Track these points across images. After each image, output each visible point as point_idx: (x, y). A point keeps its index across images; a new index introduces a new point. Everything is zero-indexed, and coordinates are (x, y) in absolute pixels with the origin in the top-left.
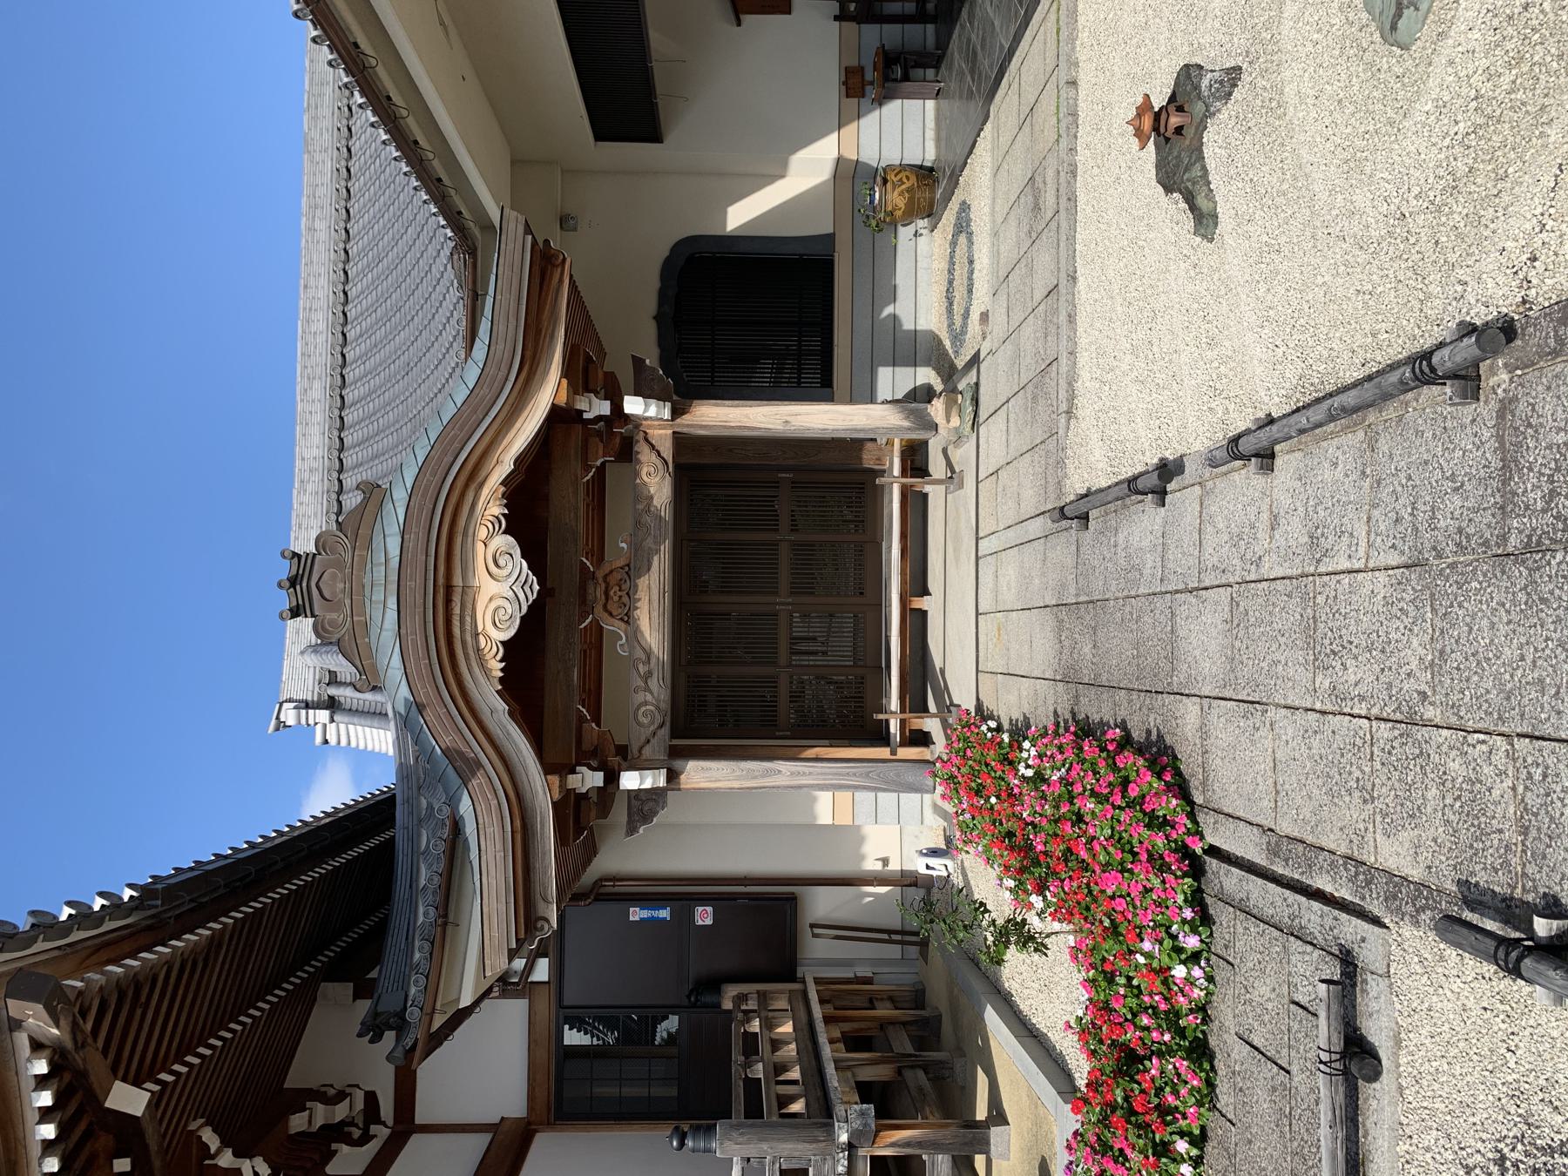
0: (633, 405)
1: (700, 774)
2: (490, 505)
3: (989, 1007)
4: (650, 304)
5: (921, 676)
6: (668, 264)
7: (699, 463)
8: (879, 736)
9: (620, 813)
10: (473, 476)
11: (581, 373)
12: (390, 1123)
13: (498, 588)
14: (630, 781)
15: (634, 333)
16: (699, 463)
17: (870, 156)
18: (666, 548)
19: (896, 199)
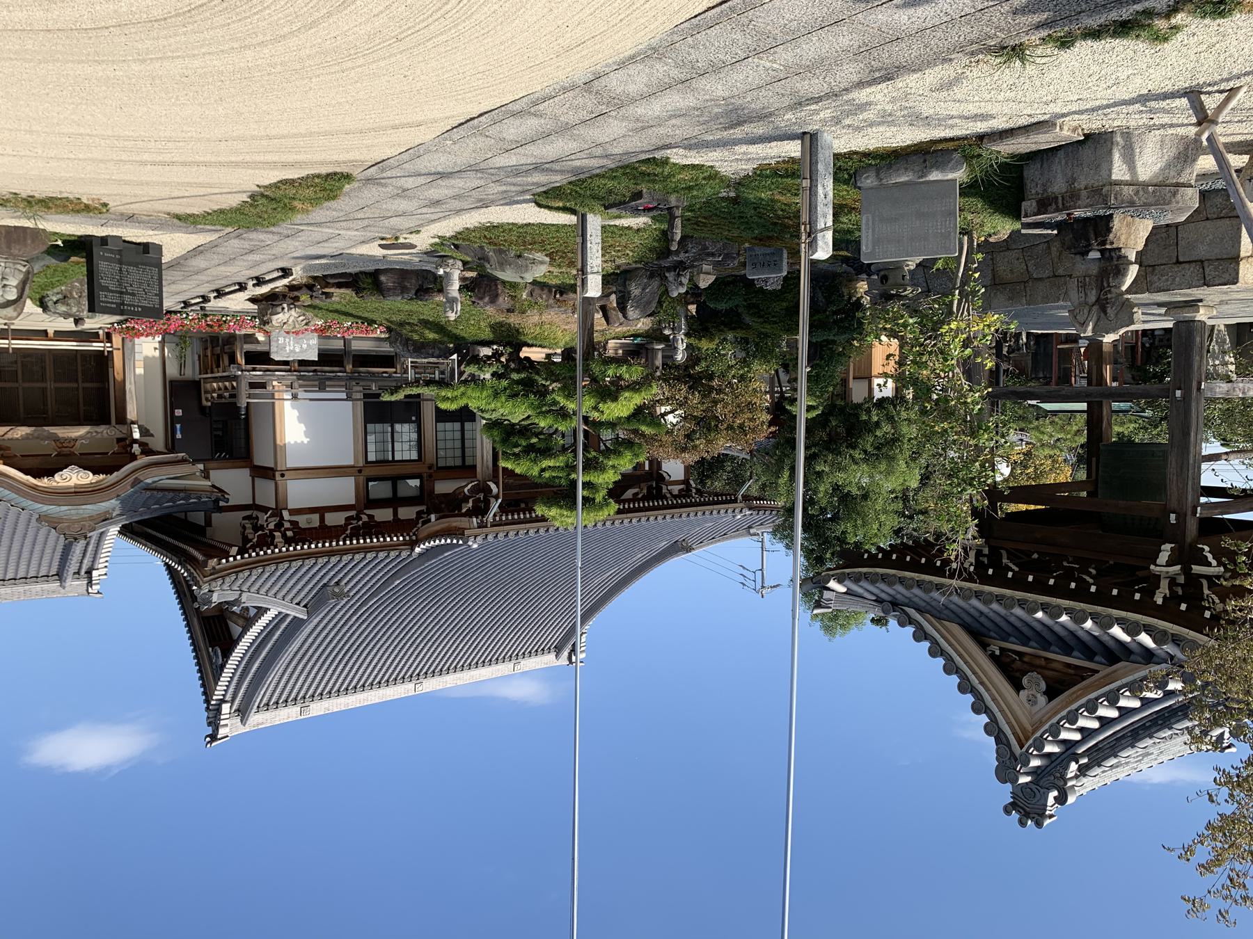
1: (132, 413)
2: (45, 482)
9: (145, 439)
10: (34, 488)
13: (73, 477)
18: (53, 430)
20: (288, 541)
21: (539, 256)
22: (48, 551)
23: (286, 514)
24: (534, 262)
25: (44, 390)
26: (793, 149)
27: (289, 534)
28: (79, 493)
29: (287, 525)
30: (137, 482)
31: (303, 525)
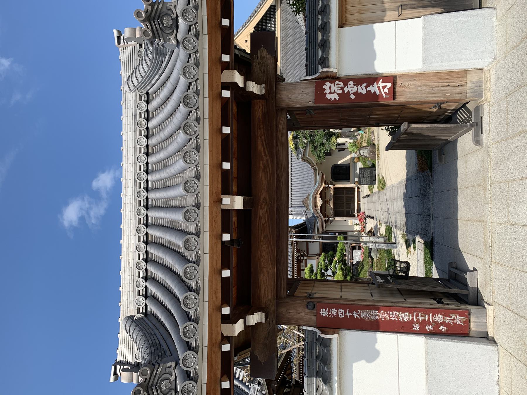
0: (330, 186)
1: (337, 219)
2: (318, 195)
3: (249, 51)
4: (330, 172)
5: (359, 210)
6: (332, 168)
7: (336, 189)
8: (354, 216)
9: (329, 222)
10: (317, 193)
11: (325, 184)
12: (241, 321)
13: (319, 202)
14: (330, 219)
15: (330, 179)
16: (336, 189)
17: (353, 156)
18: (332, 200)
19: (356, 161)
20: (298, 257)
21: (378, 256)
22: (297, 203)
23: (305, 258)
24: (376, 254)
25: (344, 194)
26: (394, 241)
27: (299, 258)
28: (315, 203)
29: (302, 258)
30: (318, 217)
31: (302, 264)
